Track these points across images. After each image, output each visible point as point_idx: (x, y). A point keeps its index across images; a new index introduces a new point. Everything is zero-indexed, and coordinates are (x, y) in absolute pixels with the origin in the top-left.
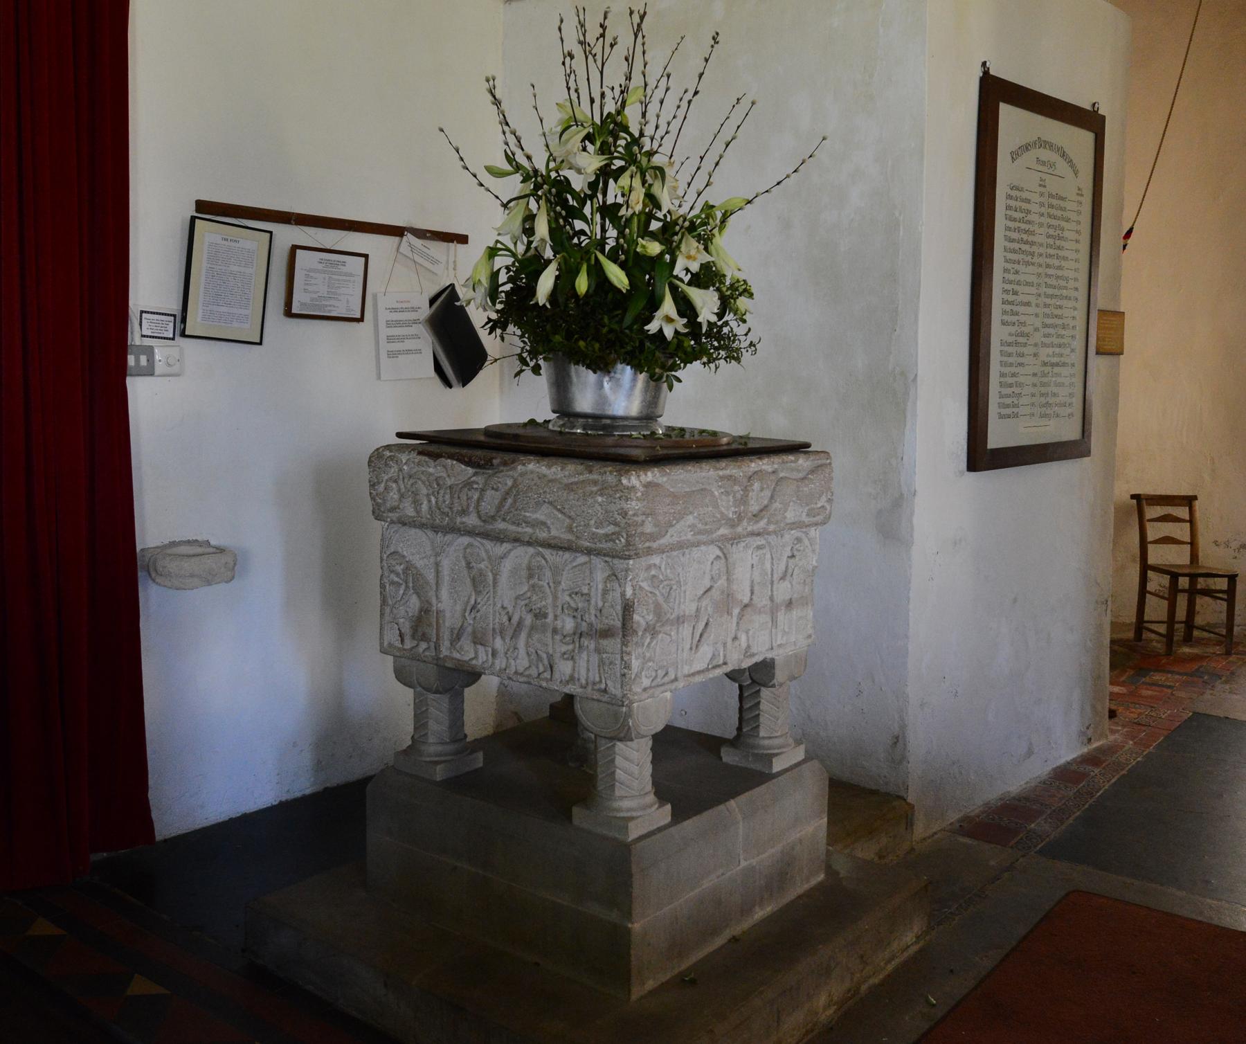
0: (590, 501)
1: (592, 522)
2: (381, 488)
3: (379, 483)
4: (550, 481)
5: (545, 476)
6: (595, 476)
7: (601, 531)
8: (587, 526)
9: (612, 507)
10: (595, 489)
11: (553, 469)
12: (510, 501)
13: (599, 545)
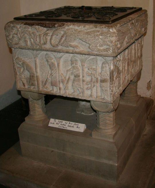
0: (97, 38)
1: (98, 45)
2: (11, 37)
4: (80, 31)
5: (77, 30)
6: (98, 29)
7: (102, 48)
8: (96, 46)
9: (106, 40)
10: (98, 33)
11: (80, 27)
13: (101, 53)
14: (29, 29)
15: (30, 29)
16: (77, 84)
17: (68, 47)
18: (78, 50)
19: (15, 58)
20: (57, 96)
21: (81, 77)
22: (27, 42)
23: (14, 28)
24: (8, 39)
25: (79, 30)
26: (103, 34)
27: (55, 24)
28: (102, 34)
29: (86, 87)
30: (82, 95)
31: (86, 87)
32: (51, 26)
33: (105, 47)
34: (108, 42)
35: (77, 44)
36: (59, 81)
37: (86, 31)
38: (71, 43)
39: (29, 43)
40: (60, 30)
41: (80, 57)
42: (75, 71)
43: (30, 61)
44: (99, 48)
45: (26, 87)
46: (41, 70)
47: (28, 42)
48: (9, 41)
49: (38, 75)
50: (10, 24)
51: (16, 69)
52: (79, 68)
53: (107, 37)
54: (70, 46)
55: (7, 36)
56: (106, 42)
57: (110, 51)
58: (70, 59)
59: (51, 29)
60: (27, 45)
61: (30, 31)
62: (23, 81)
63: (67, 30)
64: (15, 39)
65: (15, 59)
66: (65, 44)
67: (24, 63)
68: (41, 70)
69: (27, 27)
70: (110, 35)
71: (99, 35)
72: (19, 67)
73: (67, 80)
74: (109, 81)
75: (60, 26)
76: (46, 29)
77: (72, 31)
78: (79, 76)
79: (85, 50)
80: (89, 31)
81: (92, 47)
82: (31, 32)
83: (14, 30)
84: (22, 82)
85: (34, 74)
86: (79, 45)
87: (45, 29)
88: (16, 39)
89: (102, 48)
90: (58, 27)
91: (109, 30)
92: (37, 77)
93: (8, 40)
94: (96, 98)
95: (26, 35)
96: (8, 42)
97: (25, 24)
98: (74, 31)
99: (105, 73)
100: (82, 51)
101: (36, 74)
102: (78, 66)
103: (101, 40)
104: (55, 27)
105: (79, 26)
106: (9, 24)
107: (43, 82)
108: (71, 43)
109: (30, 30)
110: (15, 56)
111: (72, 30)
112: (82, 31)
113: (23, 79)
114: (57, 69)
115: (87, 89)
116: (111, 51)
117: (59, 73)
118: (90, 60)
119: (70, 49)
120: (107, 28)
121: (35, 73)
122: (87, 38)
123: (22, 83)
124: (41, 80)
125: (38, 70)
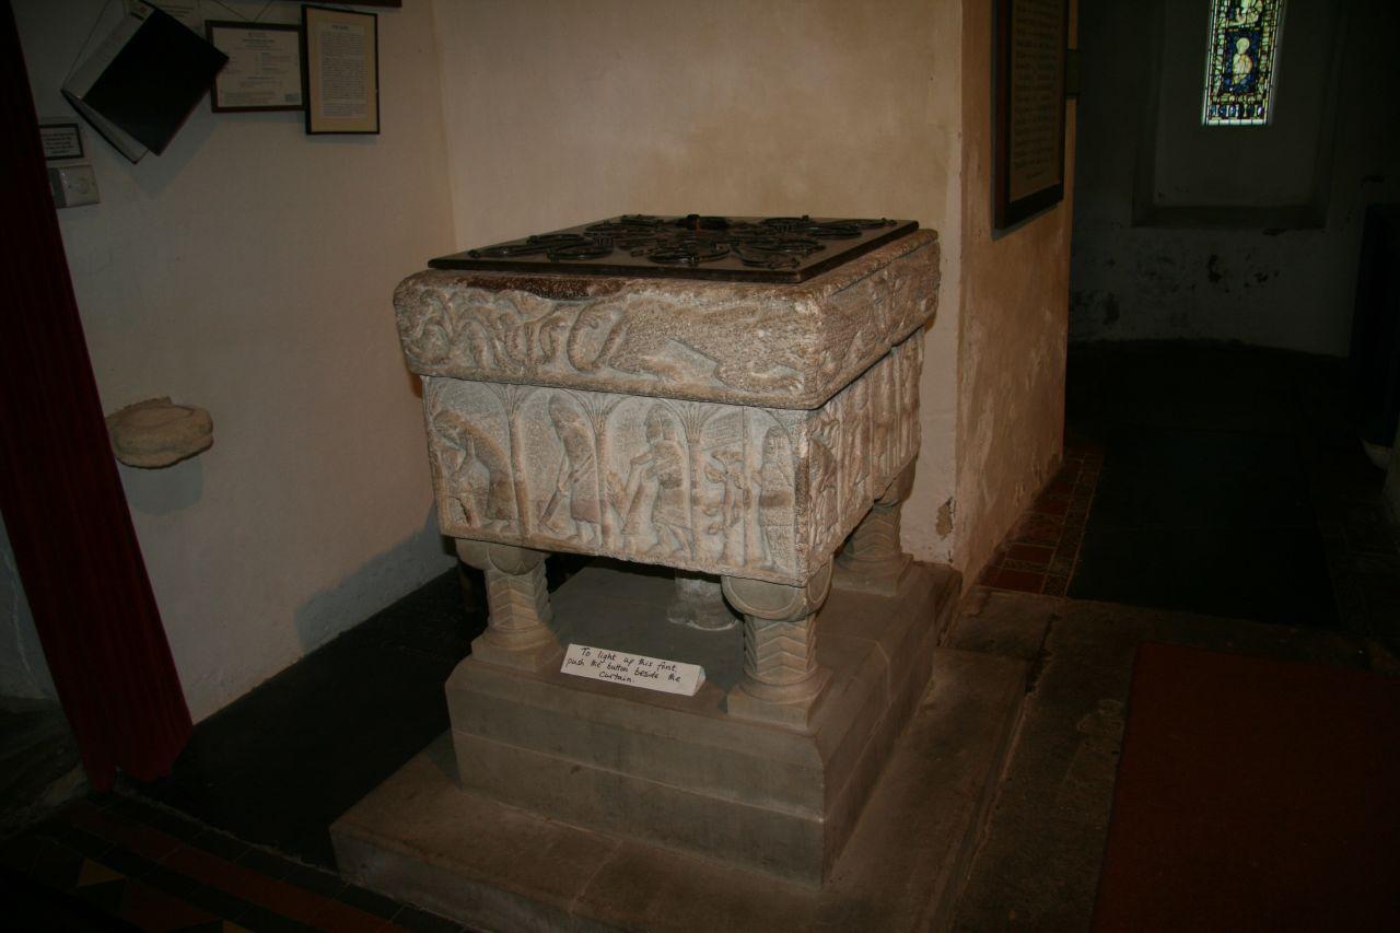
0: (746, 336)
1: (751, 364)
2: (418, 333)
5: (670, 306)
6: (749, 303)
7: (764, 376)
8: (744, 369)
9: (783, 344)
10: (751, 320)
11: (683, 296)
12: (619, 340)
13: (762, 394)
14: (487, 302)
15: (490, 304)
16: (672, 514)
17: (635, 370)
18: (674, 383)
19: (435, 414)
20: (595, 557)
21: (686, 485)
22: (481, 351)
23: (429, 300)
24: (407, 340)
25: (679, 307)
26: (771, 323)
27: (586, 284)
28: (764, 323)
29: (704, 522)
30: (689, 556)
31: (704, 522)
32: (571, 292)
33: (777, 371)
34: (788, 351)
35: (669, 360)
36: (602, 501)
37: (703, 311)
38: (647, 358)
39: (486, 356)
40: (606, 305)
41: (681, 408)
42: (662, 465)
43: (490, 426)
44: (753, 374)
45: (474, 526)
46: (532, 459)
47: (485, 353)
48: (410, 350)
49: (521, 479)
50: (414, 284)
51: (439, 454)
52: (679, 451)
53: (784, 334)
54: (644, 369)
55: (403, 328)
56: (781, 353)
57: (796, 387)
58: (643, 416)
59: (572, 302)
60: (478, 362)
61: (490, 312)
62: (464, 501)
63: (634, 305)
64: (434, 340)
65: (435, 419)
66: (623, 360)
67: (467, 433)
68: (532, 459)
69: (480, 294)
70: (795, 325)
71: (755, 326)
72: (451, 448)
73: (631, 498)
74: (793, 502)
75: (606, 292)
76: (550, 304)
77: (653, 312)
78: (678, 483)
79: (700, 383)
80: (714, 309)
81: (726, 371)
82: (495, 316)
83: (431, 308)
84: (462, 505)
85: (507, 475)
86: (678, 366)
87: (549, 303)
88: (439, 343)
89: (764, 376)
90: (596, 294)
91: (793, 307)
92: (516, 484)
93: (405, 344)
94: (744, 566)
95: (475, 325)
96: (407, 352)
97: (470, 285)
98: (658, 311)
99: (778, 472)
101: (514, 474)
102: (675, 444)
103: (761, 346)
104: (585, 294)
105: (678, 293)
106: (410, 283)
107: (539, 506)
108: (647, 358)
109: (490, 306)
110: (433, 407)
111: (650, 307)
112: (689, 310)
113: (464, 495)
114: (595, 454)
115: (709, 530)
116: (799, 386)
117: (600, 471)
118: (720, 419)
119: (645, 381)
120: (784, 298)
121: (510, 471)
122: (709, 336)
123: (461, 509)
124: (531, 496)
125: (522, 458)
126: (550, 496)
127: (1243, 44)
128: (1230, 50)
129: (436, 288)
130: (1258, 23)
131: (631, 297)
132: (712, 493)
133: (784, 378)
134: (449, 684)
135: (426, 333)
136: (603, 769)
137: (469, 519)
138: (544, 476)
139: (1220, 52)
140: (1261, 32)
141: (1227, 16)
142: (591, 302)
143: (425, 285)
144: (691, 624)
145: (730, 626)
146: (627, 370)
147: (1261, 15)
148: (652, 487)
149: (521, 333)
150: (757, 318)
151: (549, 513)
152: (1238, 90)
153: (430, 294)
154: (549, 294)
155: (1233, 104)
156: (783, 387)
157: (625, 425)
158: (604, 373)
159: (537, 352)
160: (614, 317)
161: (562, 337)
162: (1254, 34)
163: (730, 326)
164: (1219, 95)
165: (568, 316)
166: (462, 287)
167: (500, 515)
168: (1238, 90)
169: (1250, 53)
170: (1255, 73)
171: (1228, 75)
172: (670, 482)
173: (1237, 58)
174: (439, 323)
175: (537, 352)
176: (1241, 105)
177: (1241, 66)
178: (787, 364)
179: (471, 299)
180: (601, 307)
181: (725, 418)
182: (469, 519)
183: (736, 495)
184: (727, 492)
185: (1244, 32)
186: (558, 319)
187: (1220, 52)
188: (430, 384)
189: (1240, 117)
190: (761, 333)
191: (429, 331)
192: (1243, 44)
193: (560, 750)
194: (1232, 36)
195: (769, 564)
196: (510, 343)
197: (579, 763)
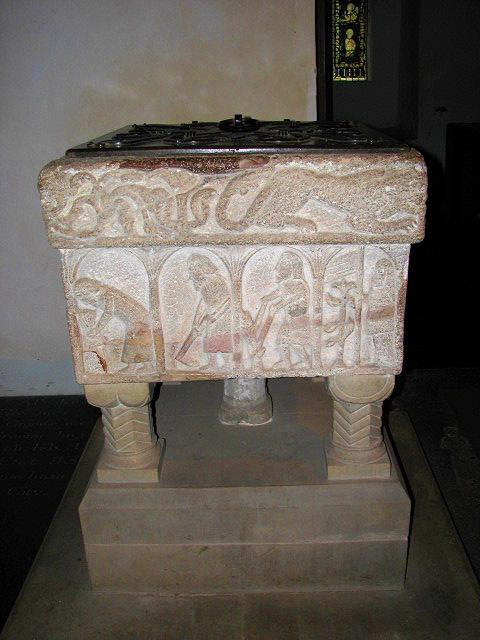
2: (65, 212)
3: (61, 207)
9: (405, 195)
10: (380, 179)
21: (311, 310)
56: (403, 202)
67: (109, 293)
78: (304, 311)
100: (326, 234)
123: (98, 360)
126: (185, 338)
127: (350, 32)
128: (343, 37)
129: (87, 171)
130: (357, 20)
131: (280, 167)
132: (330, 313)
133: (405, 220)
134: (82, 508)
135: (75, 211)
136: (229, 544)
137: (104, 367)
138: (180, 321)
139: (338, 37)
140: (359, 26)
141: (340, 15)
142: (241, 173)
143: (76, 169)
144: (243, 423)
145: (270, 420)
146: (273, 226)
147: (359, 15)
148: (280, 316)
149: (174, 203)
150: (385, 177)
151: (184, 350)
152: (349, 60)
153: (81, 177)
154: (200, 171)
155: (347, 69)
156: (404, 228)
157: (257, 271)
158: (250, 230)
159: (191, 218)
160: (262, 184)
161: (213, 203)
162: (355, 27)
163: (363, 184)
164: (339, 63)
165: (219, 185)
166: (115, 168)
167: (138, 358)
168: (349, 60)
169: (354, 38)
170: (358, 51)
171: (343, 51)
172: (298, 311)
173: (347, 40)
174: (90, 202)
175: (191, 218)
176: (352, 70)
177: (350, 46)
178: (407, 209)
179: (124, 178)
180: (252, 176)
181: (345, 256)
182: (104, 367)
183: (350, 312)
184: (343, 313)
185: (350, 25)
186: (210, 190)
187: (338, 37)
188: (70, 257)
189: (352, 77)
190: (388, 189)
191: (81, 210)
192: (350, 32)
193: (190, 538)
194: (344, 27)
195: (372, 361)
196: (163, 213)
197: (206, 545)
